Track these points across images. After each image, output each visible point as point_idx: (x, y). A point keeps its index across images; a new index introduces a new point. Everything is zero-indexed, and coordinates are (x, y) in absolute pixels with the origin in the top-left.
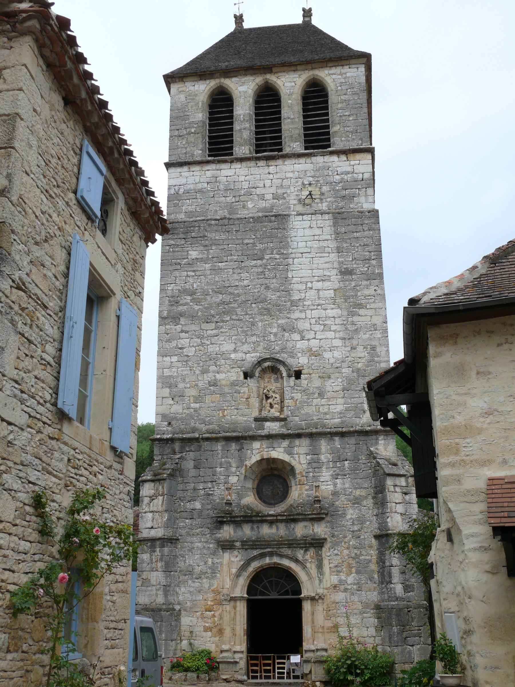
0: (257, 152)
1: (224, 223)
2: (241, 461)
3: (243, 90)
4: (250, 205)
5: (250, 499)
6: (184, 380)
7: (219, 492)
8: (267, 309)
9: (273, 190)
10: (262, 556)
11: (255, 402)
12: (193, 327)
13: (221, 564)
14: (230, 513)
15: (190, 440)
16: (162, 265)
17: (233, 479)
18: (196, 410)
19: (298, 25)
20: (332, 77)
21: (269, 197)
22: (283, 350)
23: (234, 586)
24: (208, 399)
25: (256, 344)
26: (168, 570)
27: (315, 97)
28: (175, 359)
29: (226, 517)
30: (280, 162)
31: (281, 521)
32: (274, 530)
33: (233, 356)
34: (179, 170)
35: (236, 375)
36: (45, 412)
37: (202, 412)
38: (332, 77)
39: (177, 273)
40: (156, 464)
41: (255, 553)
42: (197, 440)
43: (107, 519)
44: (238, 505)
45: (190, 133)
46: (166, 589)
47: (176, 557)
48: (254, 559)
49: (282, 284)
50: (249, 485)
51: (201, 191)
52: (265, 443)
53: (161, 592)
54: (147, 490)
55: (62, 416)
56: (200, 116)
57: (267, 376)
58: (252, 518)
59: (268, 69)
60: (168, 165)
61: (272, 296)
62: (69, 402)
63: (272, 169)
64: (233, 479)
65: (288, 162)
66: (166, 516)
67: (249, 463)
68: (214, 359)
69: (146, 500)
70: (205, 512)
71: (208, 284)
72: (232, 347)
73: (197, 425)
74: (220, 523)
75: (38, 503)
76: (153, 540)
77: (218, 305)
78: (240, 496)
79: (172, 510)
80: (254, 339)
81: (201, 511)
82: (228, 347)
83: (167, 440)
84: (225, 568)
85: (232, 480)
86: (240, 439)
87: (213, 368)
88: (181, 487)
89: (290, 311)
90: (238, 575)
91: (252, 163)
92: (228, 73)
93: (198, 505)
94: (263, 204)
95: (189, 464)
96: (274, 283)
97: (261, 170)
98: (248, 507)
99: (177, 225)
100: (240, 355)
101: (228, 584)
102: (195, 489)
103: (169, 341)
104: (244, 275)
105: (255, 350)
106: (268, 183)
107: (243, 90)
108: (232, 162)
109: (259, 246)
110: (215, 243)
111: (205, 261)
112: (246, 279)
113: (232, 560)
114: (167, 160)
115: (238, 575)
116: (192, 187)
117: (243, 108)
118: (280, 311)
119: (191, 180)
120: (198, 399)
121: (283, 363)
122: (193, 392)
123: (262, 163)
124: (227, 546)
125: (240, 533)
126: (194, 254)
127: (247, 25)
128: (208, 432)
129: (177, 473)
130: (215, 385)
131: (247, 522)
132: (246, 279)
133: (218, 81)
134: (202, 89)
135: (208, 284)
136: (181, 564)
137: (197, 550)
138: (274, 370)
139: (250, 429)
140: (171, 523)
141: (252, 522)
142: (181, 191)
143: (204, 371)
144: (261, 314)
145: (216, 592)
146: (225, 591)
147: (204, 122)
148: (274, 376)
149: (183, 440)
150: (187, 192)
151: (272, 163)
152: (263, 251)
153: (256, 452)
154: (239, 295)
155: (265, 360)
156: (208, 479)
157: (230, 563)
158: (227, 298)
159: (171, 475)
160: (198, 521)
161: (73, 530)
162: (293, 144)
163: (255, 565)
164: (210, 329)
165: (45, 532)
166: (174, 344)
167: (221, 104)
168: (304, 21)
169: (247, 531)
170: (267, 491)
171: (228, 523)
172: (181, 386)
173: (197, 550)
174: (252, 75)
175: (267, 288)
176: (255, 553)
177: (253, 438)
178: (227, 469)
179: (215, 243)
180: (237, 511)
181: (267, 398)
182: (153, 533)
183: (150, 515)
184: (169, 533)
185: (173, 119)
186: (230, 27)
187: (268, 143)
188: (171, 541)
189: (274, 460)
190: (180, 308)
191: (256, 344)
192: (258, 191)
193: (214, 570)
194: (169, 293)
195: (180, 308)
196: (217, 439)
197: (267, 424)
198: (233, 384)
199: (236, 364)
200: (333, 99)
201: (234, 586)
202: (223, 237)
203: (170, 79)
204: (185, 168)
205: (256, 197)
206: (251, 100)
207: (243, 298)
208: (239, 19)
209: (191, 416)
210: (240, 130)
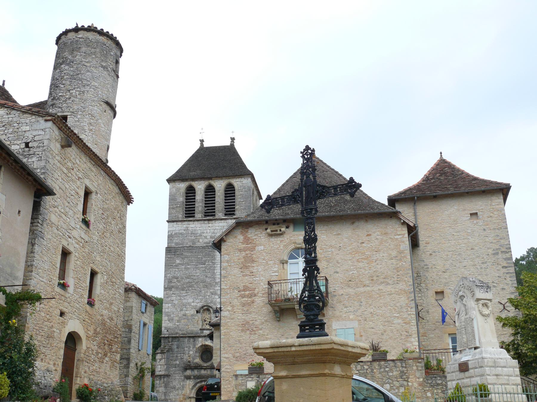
0: (205, 216)
1: (191, 248)
2: (194, 346)
3: (200, 187)
4: (201, 241)
5: (198, 360)
6: (173, 314)
7: (186, 358)
8: (206, 286)
9: (210, 234)
10: (201, 382)
11: (200, 323)
12: (177, 292)
13: (186, 385)
14: (189, 365)
15: (175, 337)
16: (165, 266)
17: (191, 353)
18: (178, 326)
19: (228, 146)
20: (237, 183)
21: (209, 237)
22: (211, 302)
23: (191, 393)
24: (182, 321)
25: (201, 299)
26: (166, 387)
27: (230, 190)
28: (170, 305)
29: (188, 367)
30: (213, 222)
31: (209, 368)
32: (206, 372)
33: (192, 304)
34: (172, 224)
35: (193, 312)
36: (137, 350)
37: (180, 326)
38: (237, 183)
39: (171, 269)
40: (162, 346)
41: (199, 380)
42: (178, 337)
43: (146, 367)
44: (193, 362)
45: (177, 207)
46: (165, 394)
47: (169, 382)
48: (198, 383)
49: (212, 275)
50: (198, 355)
51: (181, 234)
52: (204, 339)
53: (163, 395)
54: (158, 357)
55: (139, 350)
56: (181, 199)
57: (206, 312)
58: (198, 367)
59: (210, 179)
60: (168, 221)
61: (208, 280)
62: (140, 348)
63: (210, 225)
64: (191, 353)
65: (217, 222)
66: (166, 367)
67: (197, 346)
68: (184, 305)
69: (158, 360)
70: (180, 365)
71: (183, 274)
72: (192, 300)
73: (178, 331)
74: (186, 369)
75: (136, 364)
76: (160, 376)
77: (187, 283)
78: (194, 359)
79: (168, 365)
80: (201, 297)
81: (179, 365)
82: (191, 300)
83: (167, 337)
84: (187, 386)
85: (190, 353)
86: (194, 337)
87: (184, 309)
88: (171, 355)
89: (215, 286)
90: (192, 389)
91: (202, 222)
92: (193, 180)
93: (178, 362)
94: (206, 240)
95: (175, 347)
96: (209, 275)
97: (206, 225)
98: (196, 363)
99: (171, 249)
100: (195, 304)
101: (188, 392)
102: (177, 356)
103: (167, 298)
104: (198, 271)
105: (201, 302)
106: (208, 231)
107: (200, 187)
108: (194, 221)
109: (204, 259)
110: (187, 257)
111: (182, 264)
112: (198, 273)
113: (190, 383)
114: (167, 219)
115: (192, 389)
116: (178, 232)
117: (200, 196)
118: (211, 286)
119: (177, 229)
120: (179, 321)
121: (211, 307)
122: (177, 318)
123: (206, 222)
124: (188, 378)
125: (193, 373)
126: (178, 261)
127: (206, 145)
128: (182, 334)
129: (170, 350)
130: (185, 316)
131: (196, 369)
132: (198, 273)
133: (189, 183)
134: (183, 186)
135: (183, 274)
136: (171, 385)
137: (177, 380)
138: (208, 310)
139: (198, 333)
140: (167, 369)
141: (198, 369)
142: (173, 233)
143: (181, 310)
144: (204, 287)
145: (184, 395)
146: (187, 395)
147: (183, 202)
148: (208, 312)
149: (172, 337)
150: (176, 234)
151: (210, 222)
152: (205, 261)
153: (201, 342)
154: (195, 279)
155: (205, 306)
156: (182, 352)
157: (189, 384)
158: (191, 280)
159: (168, 351)
160: (178, 368)
161: (141, 369)
162: (220, 214)
163: (199, 385)
164: (184, 293)
165: (137, 369)
166: (169, 299)
167: (191, 190)
168: (231, 144)
169: (196, 372)
170: (205, 357)
171: (189, 369)
172: (172, 316)
173: (177, 380)
174: (203, 180)
175: (206, 277)
176: (199, 380)
177: (199, 337)
178: (189, 348)
179: (187, 257)
180: (192, 365)
181: (205, 321)
182: (161, 373)
183: (159, 366)
184: (167, 373)
185: (170, 200)
186: (197, 146)
187: (210, 214)
188: (168, 376)
189: (207, 345)
190: (172, 284)
191: (201, 299)
192: (204, 235)
193: (183, 387)
194: (168, 278)
195: (172, 284)
196: (185, 337)
197: (205, 331)
198: (192, 315)
199: (193, 307)
200: (237, 193)
201: (191, 393)
202: (190, 254)
203: (169, 181)
204: (175, 223)
205: (203, 237)
206: (203, 192)
207: (197, 281)
208: (202, 141)
209: (176, 328)
210: (198, 207)
